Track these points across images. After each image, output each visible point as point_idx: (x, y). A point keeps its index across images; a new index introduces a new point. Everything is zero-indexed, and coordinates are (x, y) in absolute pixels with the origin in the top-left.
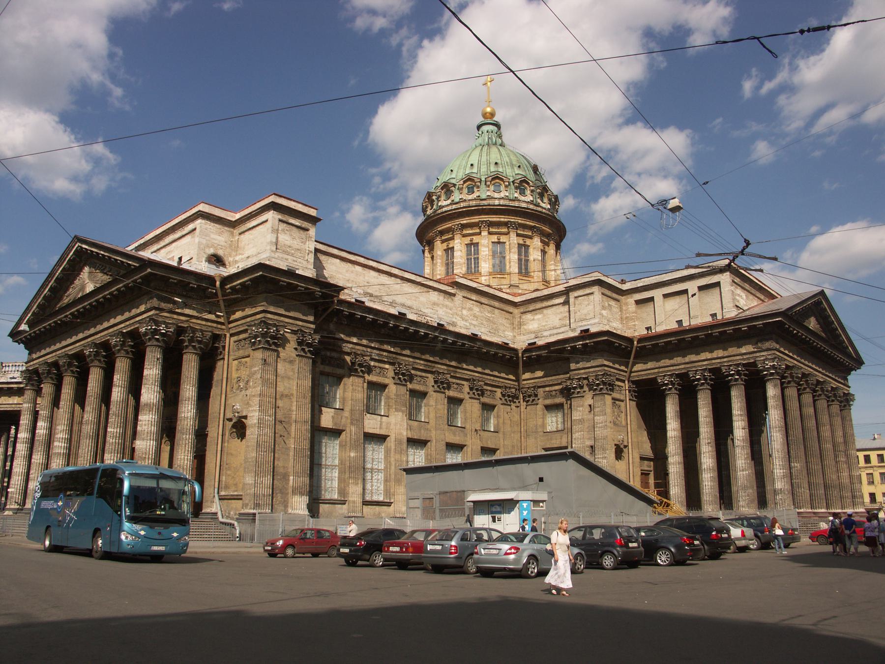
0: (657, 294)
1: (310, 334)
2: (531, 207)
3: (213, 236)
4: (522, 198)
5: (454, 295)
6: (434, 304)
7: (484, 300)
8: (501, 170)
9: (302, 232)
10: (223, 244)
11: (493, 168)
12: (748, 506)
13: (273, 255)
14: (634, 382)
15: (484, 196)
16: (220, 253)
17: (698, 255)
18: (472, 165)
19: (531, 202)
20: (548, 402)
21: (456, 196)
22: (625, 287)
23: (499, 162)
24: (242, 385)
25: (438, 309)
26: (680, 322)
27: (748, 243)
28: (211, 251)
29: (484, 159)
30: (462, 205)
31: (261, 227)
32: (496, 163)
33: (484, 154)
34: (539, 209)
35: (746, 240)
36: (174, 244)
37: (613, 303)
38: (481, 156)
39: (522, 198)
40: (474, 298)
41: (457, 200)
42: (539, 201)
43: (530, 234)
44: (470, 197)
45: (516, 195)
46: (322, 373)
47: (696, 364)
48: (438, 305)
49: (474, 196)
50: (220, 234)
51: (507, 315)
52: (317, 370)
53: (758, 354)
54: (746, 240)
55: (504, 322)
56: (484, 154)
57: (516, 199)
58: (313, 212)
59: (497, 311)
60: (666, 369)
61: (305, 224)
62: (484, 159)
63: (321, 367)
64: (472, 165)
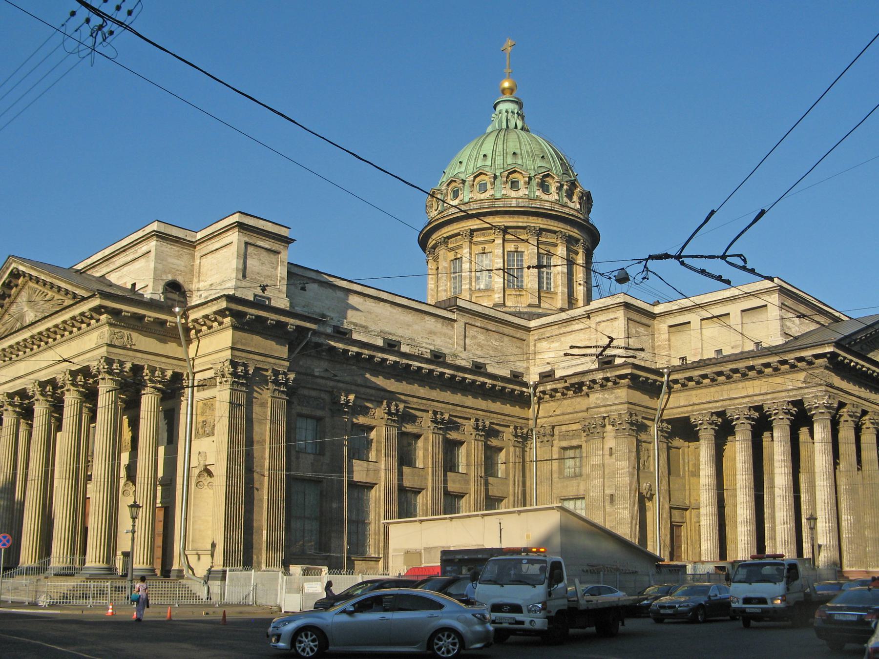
0: (694, 318)
1: (285, 374)
2: (557, 207)
3: (170, 260)
4: (545, 197)
5: (455, 321)
6: (431, 333)
7: (491, 326)
8: (520, 162)
9: (272, 256)
10: (182, 268)
11: (510, 160)
12: (515, 574)
13: (239, 284)
14: (669, 421)
15: (498, 196)
16: (180, 279)
17: (572, 347)
18: (485, 156)
19: (557, 202)
20: (565, 444)
21: (466, 195)
22: (657, 310)
23: (518, 151)
24: (208, 430)
25: (435, 338)
26: (719, 352)
27: (612, 340)
28: (170, 277)
29: (500, 148)
30: (473, 206)
31: (224, 250)
32: (514, 153)
33: (500, 142)
34: (567, 210)
35: (609, 337)
36: (126, 268)
37: (641, 330)
38: (495, 144)
39: (545, 197)
40: (479, 325)
41: (466, 200)
42: (565, 199)
43: (554, 241)
44: (482, 196)
45: (538, 193)
46: (300, 415)
47: (736, 401)
48: (435, 333)
49: (487, 195)
50: (179, 257)
51: (519, 343)
52: (294, 412)
53: (806, 391)
54: (609, 337)
55: (516, 351)
56: (500, 142)
57: (537, 198)
58: (284, 232)
59: (506, 339)
60: (702, 406)
61: (276, 246)
62: (500, 148)
63: (298, 409)
64: (485, 156)
